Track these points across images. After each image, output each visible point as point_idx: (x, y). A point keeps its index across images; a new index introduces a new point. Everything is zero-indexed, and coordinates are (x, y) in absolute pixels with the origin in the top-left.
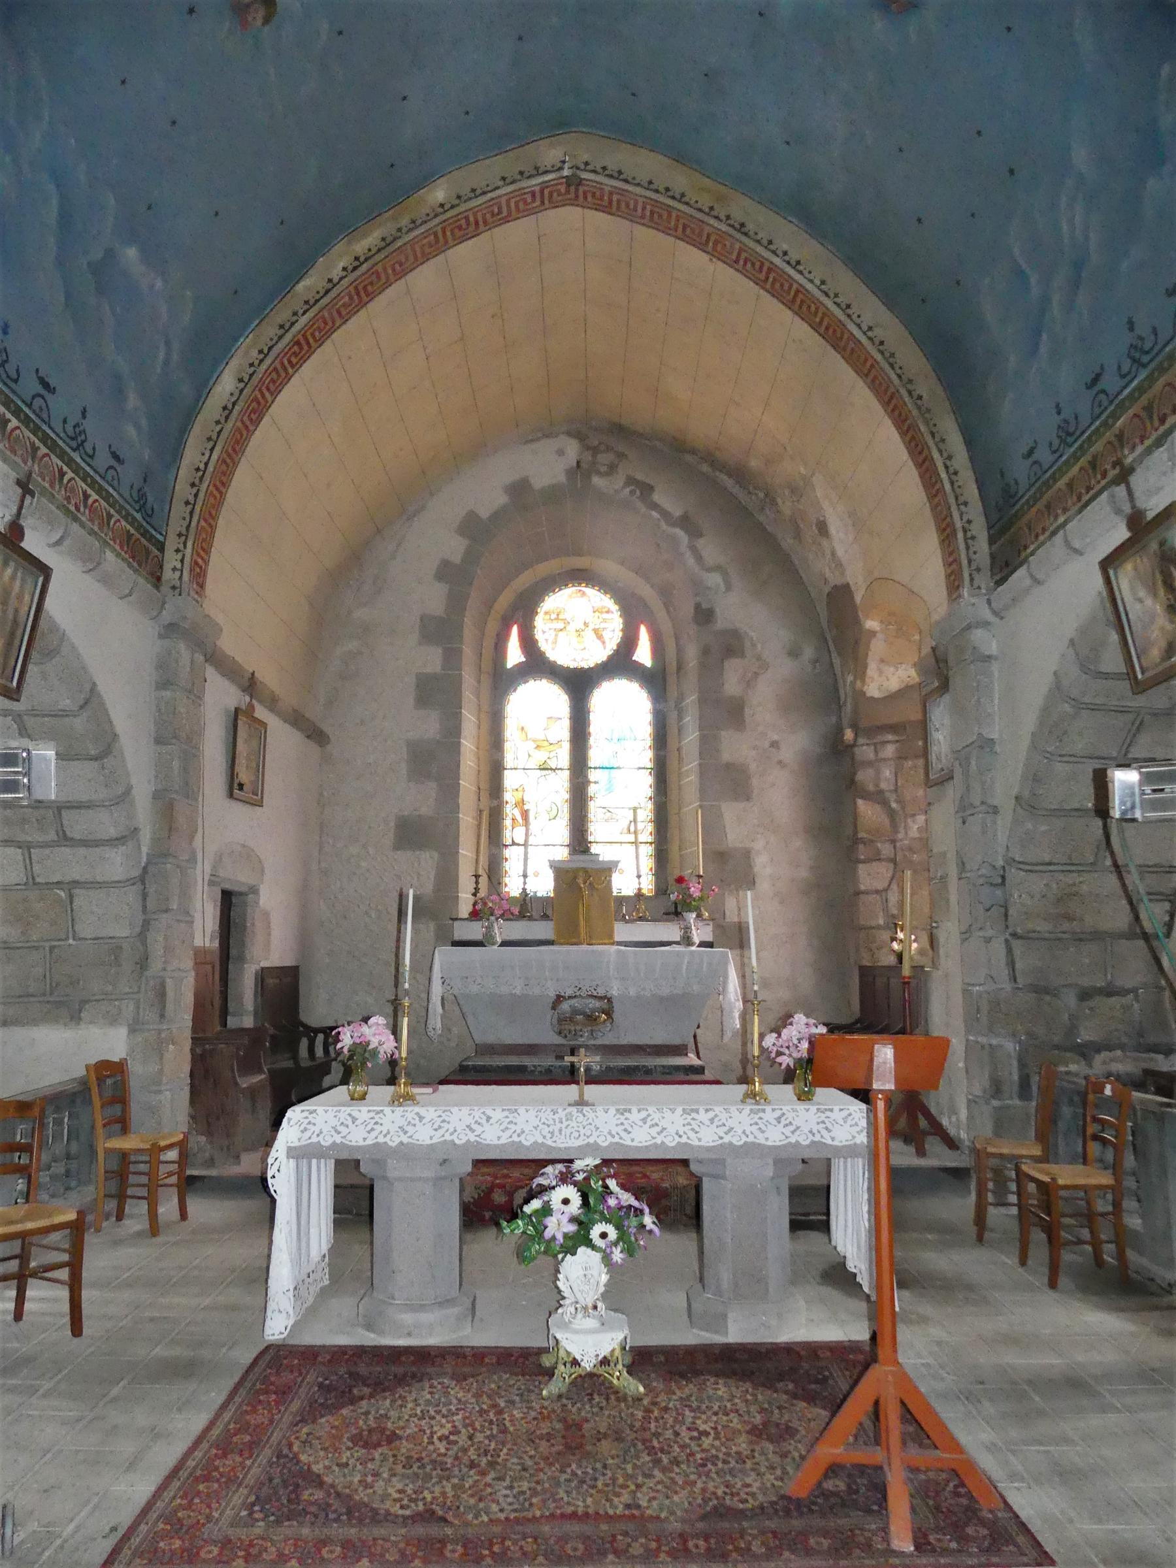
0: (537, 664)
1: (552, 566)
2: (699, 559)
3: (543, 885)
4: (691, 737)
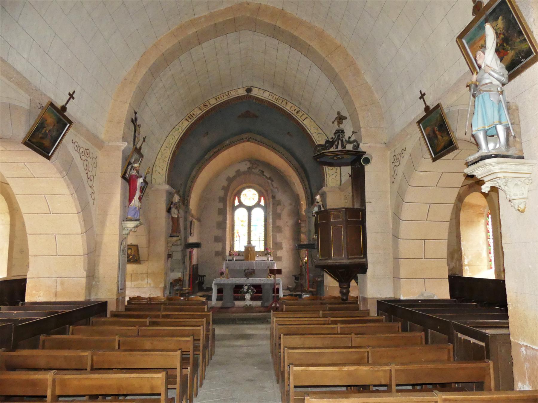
0: (241, 205)
1: (244, 185)
2: (272, 185)
3: (243, 249)
4: (271, 221)
